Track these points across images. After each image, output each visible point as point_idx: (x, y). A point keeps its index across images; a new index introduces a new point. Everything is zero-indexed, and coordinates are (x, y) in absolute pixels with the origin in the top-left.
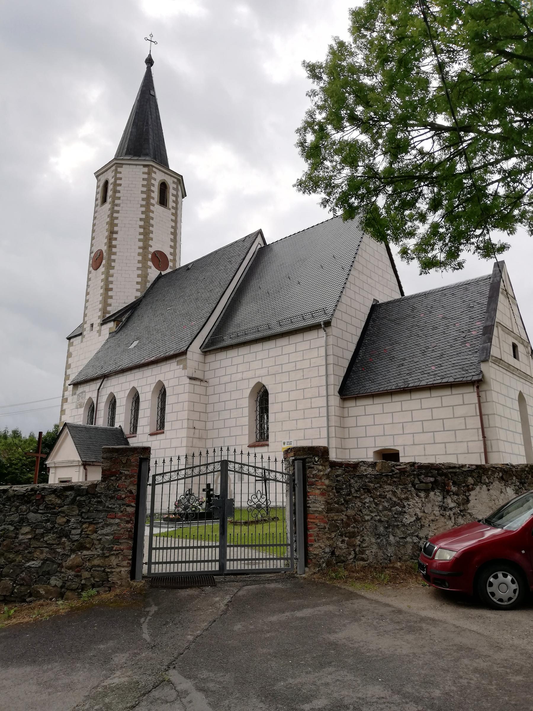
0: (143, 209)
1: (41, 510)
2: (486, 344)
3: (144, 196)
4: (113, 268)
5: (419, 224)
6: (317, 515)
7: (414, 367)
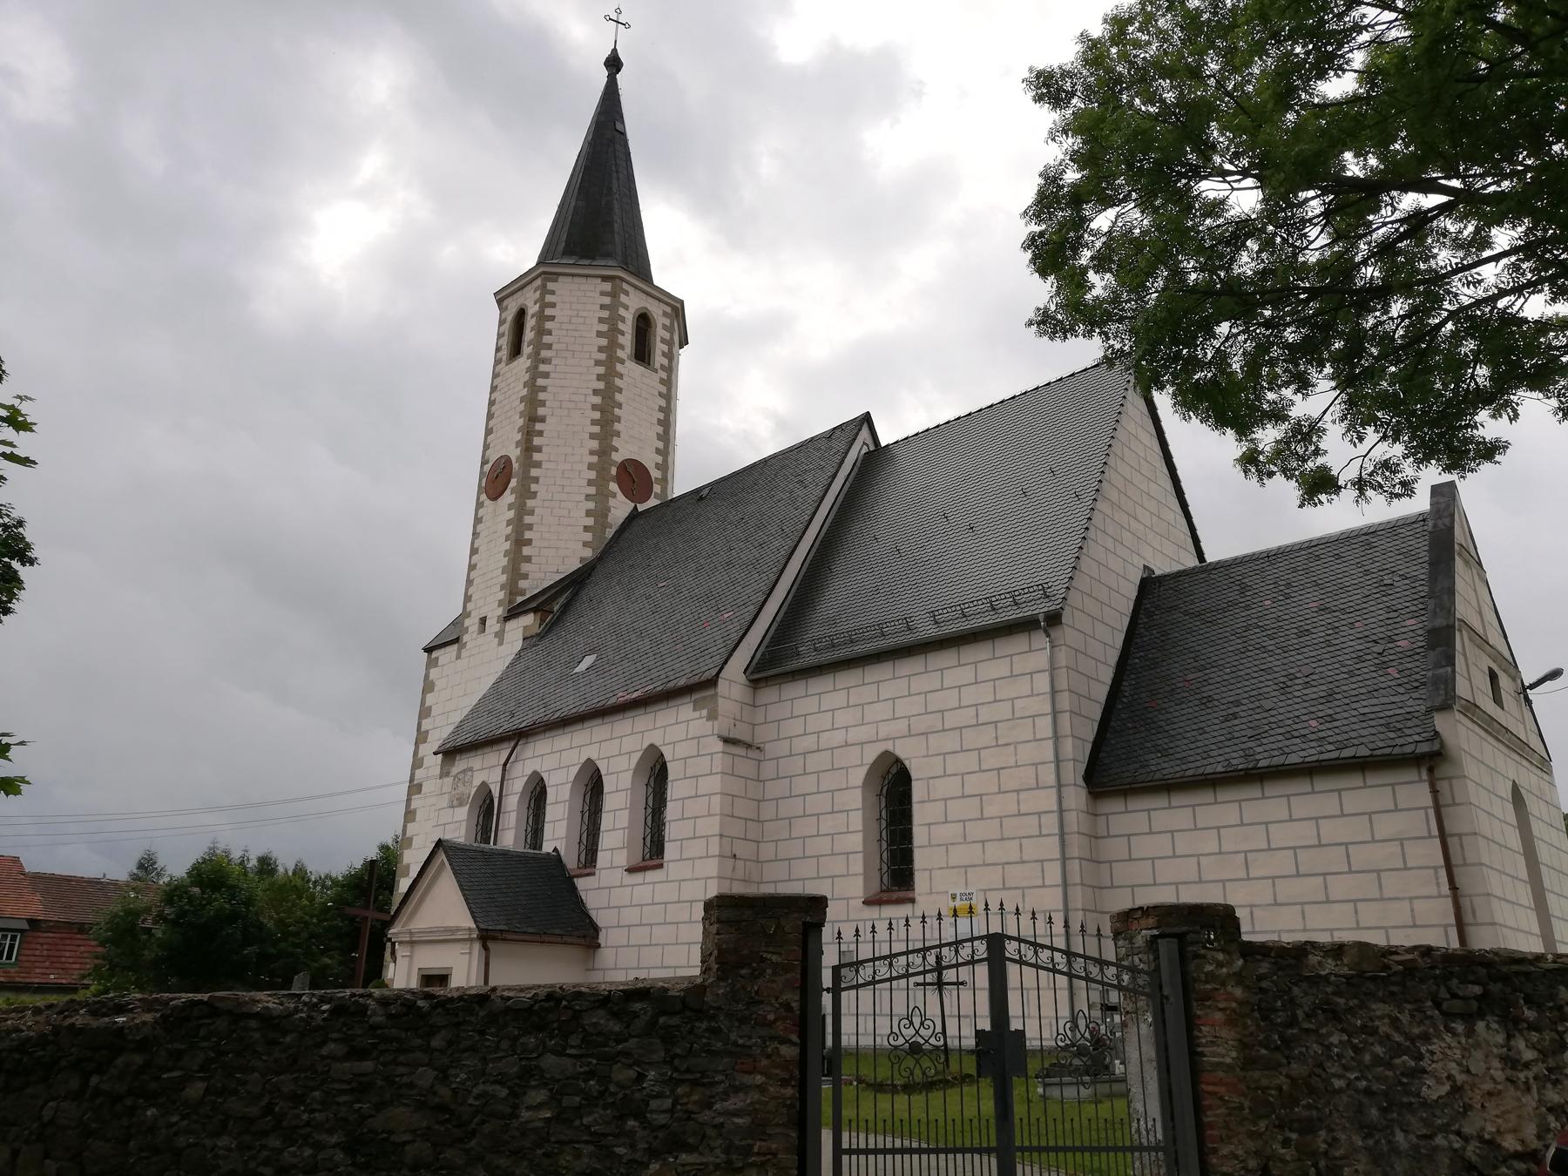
3: (604, 342)
4: (534, 495)
5: (1294, 398)
6: (1221, 1074)
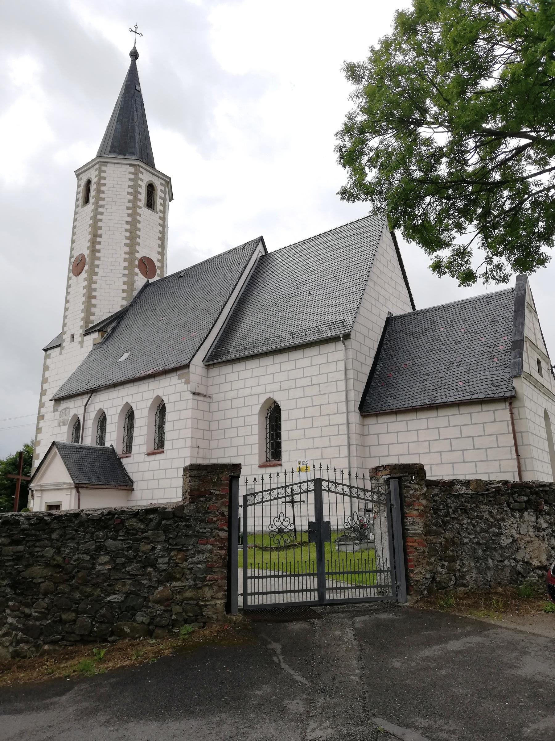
0: (130, 212)
1: (120, 536)
2: (517, 360)
3: (131, 197)
4: (97, 274)
6: (416, 538)
7: (439, 383)
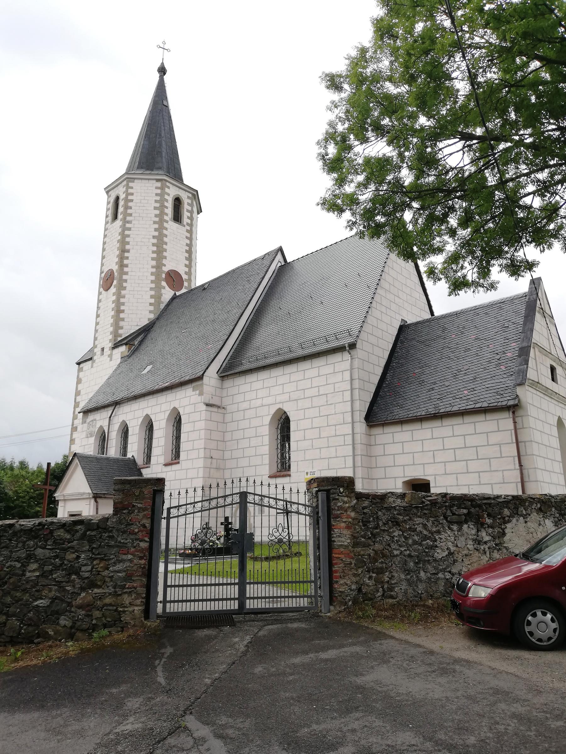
0: (156, 226)
2: (522, 367)
3: (157, 212)
4: (125, 288)
6: (342, 550)
7: (445, 391)
